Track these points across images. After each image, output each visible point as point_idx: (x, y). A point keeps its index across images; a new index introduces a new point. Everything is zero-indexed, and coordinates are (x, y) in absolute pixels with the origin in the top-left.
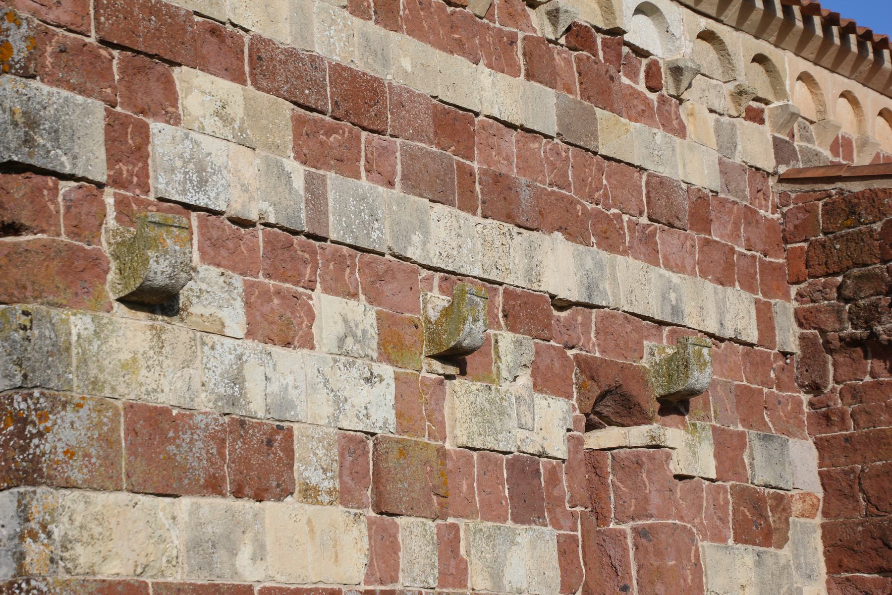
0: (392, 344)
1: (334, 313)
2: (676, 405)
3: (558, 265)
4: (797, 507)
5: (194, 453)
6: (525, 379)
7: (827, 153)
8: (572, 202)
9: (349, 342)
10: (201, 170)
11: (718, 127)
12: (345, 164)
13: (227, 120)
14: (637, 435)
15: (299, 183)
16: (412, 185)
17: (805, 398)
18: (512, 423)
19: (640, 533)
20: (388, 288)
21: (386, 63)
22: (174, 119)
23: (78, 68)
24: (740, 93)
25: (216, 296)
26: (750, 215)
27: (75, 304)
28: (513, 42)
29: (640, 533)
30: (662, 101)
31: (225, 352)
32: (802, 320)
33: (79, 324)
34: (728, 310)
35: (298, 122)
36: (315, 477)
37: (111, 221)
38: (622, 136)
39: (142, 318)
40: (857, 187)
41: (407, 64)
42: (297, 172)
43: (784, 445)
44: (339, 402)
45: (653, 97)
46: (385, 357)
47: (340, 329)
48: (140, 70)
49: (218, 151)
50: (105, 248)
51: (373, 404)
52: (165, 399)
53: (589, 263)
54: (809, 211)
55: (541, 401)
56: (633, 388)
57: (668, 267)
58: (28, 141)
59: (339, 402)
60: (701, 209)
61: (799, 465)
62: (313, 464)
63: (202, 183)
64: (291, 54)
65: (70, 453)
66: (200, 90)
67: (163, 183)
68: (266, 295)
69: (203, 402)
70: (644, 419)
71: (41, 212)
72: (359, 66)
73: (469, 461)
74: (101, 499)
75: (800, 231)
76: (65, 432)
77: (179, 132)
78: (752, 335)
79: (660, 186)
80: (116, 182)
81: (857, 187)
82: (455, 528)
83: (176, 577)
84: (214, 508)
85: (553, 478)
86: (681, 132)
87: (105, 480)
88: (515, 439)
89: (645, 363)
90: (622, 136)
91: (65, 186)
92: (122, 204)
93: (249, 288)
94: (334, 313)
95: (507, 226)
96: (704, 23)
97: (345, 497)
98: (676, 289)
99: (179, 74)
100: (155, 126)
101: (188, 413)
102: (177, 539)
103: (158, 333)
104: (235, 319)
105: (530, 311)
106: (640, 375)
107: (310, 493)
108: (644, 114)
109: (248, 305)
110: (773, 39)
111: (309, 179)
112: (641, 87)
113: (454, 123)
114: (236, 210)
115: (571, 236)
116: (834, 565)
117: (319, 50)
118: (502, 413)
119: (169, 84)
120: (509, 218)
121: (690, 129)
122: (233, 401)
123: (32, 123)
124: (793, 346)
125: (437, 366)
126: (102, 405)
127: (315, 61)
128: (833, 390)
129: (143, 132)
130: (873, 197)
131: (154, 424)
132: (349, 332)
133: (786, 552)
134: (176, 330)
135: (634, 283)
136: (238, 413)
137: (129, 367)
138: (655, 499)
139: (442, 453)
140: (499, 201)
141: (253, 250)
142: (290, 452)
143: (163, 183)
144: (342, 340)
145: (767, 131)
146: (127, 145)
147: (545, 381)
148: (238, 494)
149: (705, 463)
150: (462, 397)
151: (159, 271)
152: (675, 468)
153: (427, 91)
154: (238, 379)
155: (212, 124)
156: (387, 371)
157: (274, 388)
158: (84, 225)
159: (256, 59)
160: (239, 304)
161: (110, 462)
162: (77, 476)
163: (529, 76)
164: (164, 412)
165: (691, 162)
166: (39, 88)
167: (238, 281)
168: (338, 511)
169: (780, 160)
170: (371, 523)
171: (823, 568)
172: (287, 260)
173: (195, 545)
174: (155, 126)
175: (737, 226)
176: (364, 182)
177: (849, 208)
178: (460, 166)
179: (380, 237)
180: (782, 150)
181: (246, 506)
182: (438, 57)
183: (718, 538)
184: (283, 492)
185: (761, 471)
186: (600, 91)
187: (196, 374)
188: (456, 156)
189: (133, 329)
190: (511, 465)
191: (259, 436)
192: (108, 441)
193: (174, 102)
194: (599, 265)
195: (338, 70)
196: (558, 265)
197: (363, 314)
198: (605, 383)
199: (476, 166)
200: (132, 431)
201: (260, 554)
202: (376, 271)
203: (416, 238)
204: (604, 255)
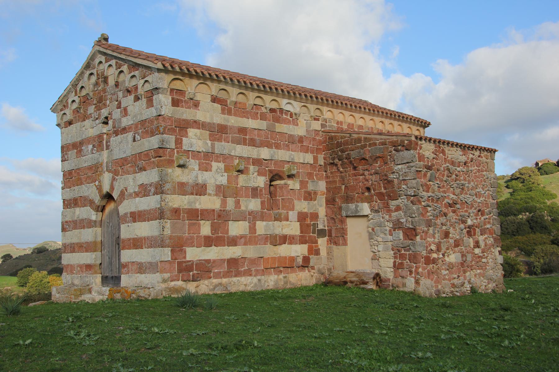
0: (227, 169)
1: (215, 165)
2: (290, 176)
3: (265, 153)
4: (319, 194)
5: (189, 189)
6: (256, 174)
7: (336, 125)
8: (269, 141)
9: (218, 170)
10: (191, 144)
11: (307, 123)
12: (219, 140)
13: (196, 136)
14: (282, 182)
15: (210, 145)
16: (233, 142)
17: (324, 173)
18: (252, 182)
19: (282, 199)
20: (227, 160)
21: (228, 122)
22: (187, 137)
23: (171, 131)
24: (311, 117)
25: (193, 164)
26: (314, 139)
27: (170, 167)
28: (258, 113)
29: (282, 199)
30: (293, 120)
31: (194, 173)
32: (325, 159)
33: (170, 170)
34: (309, 158)
35: (210, 134)
36: (211, 192)
37: (176, 154)
38: (281, 128)
39: (180, 169)
40: (333, 134)
41: (233, 121)
42: (209, 143)
43: (317, 182)
44: (216, 180)
45: (291, 119)
46: (225, 171)
47: (217, 168)
48: (182, 130)
49: (194, 141)
50: (175, 159)
51: (223, 180)
52: (183, 181)
53: (272, 152)
54: (326, 138)
55: (259, 177)
56: (281, 174)
57: (292, 151)
58: (162, 144)
59: (216, 180)
60: (301, 139)
61: (322, 186)
62: (210, 190)
63: (191, 147)
64: (209, 123)
65: (168, 189)
66: (192, 132)
67: (185, 148)
68: (203, 163)
69: (191, 181)
70: (284, 179)
71: (165, 154)
72: (223, 123)
73: (243, 188)
74: (173, 196)
75: (325, 142)
76: (167, 186)
77: (187, 139)
78: (312, 162)
79: (291, 136)
80: (177, 148)
81: (333, 134)
82: (239, 200)
83: (186, 207)
84: (192, 197)
85: (261, 190)
86: (297, 125)
87: (174, 193)
88: (252, 184)
89: (285, 169)
90: (281, 128)
91: (168, 150)
92: (178, 152)
93: (199, 163)
94: (215, 165)
95: (253, 147)
96: (303, 104)
97: (216, 195)
98: (293, 155)
99: (189, 130)
100: (184, 139)
101: (188, 183)
102: (186, 202)
103: (183, 171)
104: (197, 168)
105: (257, 162)
106: (283, 172)
107: (210, 195)
108: (288, 122)
109: (199, 165)
110: (67, 197)
111: (212, 144)
112: (289, 117)
113: (243, 130)
114: (198, 150)
115: (268, 147)
116: (327, 204)
117: (215, 122)
118: (250, 180)
119: (186, 131)
120: (254, 146)
121: (299, 124)
122: (196, 181)
123: (163, 141)
124: (323, 164)
125: (236, 173)
126: (173, 182)
127: (214, 124)
128: (375, 166)
129: (182, 139)
130: (335, 136)
131: (182, 185)
132: (218, 168)
133: (316, 202)
134: (186, 171)
135: (282, 155)
136: (197, 182)
137: (178, 176)
138: (285, 194)
139: (237, 187)
140: (253, 143)
141: (201, 156)
142: (206, 188)
143: (185, 148)
144: (217, 170)
145: (320, 122)
146: (179, 142)
147: (260, 174)
148: (196, 195)
149: (297, 186)
150: (242, 177)
151: (181, 162)
152: (290, 188)
153: (237, 125)
154: (197, 177)
155: (194, 137)
156: (226, 174)
157: (203, 178)
158: (171, 155)
159: (203, 125)
160: (197, 165)
161: (174, 190)
162: (169, 193)
163: (261, 119)
164: (184, 183)
165: (299, 131)
166: (165, 135)
167: (197, 161)
168: (215, 197)
169: (322, 128)
170: (221, 199)
171: (325, 204)
172: (206, 159)
173: (188, 203)
174: (184, 139)
175: (310, 141)
176: (223, 143)
177: (331, 138)
178: (244, 138)
179: (225, 152)
180: (323, 126)
181: (198, 197)
182: (240, 119)
183: (299, 199)
184: (205, 194)
185: (311, 187)
186: (277, 120)
187: (189, 177)
188: (243, 136)
189: (179, 171)
190: (252, 189)
191: (200, 186)
192: (174, 188)
193: (187, 134)
194: (274, 152)
195: (218, 125)
196: (265, 153)
197: (222, 165)
198: (274, 173)
199: (247, 137)
200: (178, 186)
201: (200, 204)
202: (225, 158)
203: (233, 151)
204: (276, 150)
